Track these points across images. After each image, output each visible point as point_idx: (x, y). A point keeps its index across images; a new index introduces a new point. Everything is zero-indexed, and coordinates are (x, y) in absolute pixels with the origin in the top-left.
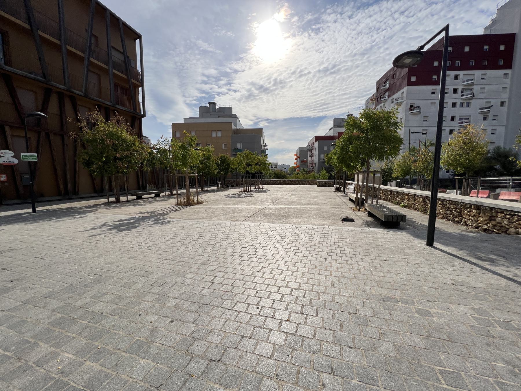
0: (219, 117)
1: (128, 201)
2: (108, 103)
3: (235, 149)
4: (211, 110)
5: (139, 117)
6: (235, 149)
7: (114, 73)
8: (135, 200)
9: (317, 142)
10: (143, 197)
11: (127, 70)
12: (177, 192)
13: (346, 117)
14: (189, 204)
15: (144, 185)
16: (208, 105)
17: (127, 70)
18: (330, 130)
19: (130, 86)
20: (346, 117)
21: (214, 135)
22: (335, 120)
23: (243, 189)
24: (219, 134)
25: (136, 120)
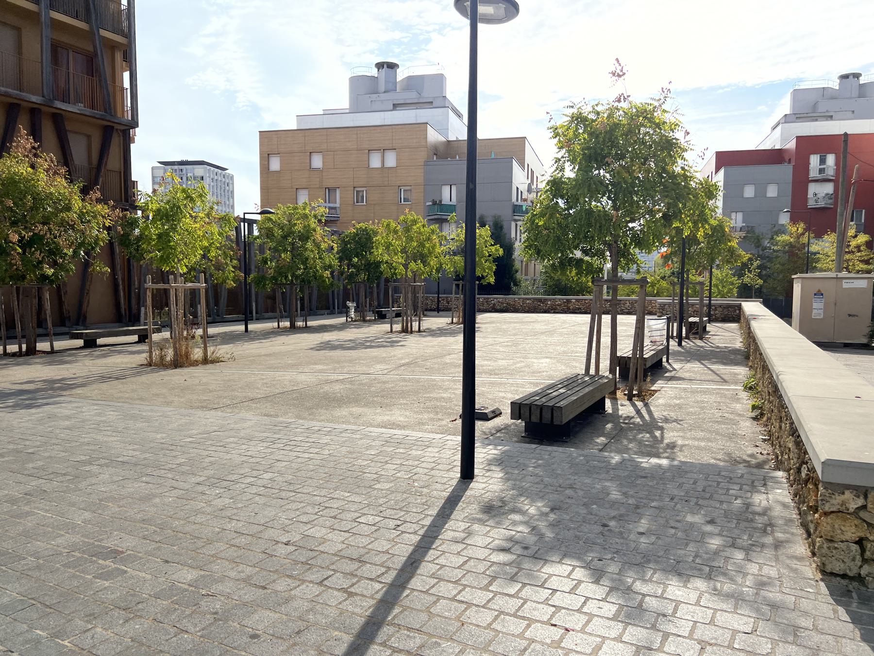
0: (395, 106)
1: (52, 352)
2: (34, 99)
3: (434, 203)
4: (382, 88)
5: (123, 128)
6: (434, 203)
7: (53, 20)
8: (81, 348)
9: (722, 172)
10: (100, 341)
11: (88, 10)
12: (205, 331)
13: (835, 84)
14: (180, 362)
15: (134, 311)
16: (374, 72)
17: (88, 10)
18: (774, 128)
19: (95, 47)
20: (835, 84)
21: (375, 162)
22: (797, 94)
23: (397, 327)
24: (391, 160)
25: (115, 135)
